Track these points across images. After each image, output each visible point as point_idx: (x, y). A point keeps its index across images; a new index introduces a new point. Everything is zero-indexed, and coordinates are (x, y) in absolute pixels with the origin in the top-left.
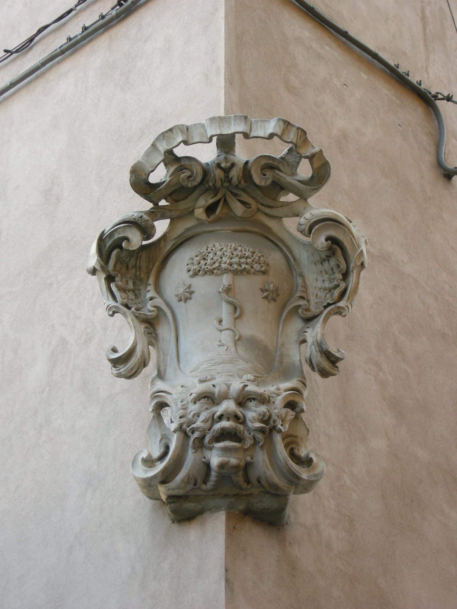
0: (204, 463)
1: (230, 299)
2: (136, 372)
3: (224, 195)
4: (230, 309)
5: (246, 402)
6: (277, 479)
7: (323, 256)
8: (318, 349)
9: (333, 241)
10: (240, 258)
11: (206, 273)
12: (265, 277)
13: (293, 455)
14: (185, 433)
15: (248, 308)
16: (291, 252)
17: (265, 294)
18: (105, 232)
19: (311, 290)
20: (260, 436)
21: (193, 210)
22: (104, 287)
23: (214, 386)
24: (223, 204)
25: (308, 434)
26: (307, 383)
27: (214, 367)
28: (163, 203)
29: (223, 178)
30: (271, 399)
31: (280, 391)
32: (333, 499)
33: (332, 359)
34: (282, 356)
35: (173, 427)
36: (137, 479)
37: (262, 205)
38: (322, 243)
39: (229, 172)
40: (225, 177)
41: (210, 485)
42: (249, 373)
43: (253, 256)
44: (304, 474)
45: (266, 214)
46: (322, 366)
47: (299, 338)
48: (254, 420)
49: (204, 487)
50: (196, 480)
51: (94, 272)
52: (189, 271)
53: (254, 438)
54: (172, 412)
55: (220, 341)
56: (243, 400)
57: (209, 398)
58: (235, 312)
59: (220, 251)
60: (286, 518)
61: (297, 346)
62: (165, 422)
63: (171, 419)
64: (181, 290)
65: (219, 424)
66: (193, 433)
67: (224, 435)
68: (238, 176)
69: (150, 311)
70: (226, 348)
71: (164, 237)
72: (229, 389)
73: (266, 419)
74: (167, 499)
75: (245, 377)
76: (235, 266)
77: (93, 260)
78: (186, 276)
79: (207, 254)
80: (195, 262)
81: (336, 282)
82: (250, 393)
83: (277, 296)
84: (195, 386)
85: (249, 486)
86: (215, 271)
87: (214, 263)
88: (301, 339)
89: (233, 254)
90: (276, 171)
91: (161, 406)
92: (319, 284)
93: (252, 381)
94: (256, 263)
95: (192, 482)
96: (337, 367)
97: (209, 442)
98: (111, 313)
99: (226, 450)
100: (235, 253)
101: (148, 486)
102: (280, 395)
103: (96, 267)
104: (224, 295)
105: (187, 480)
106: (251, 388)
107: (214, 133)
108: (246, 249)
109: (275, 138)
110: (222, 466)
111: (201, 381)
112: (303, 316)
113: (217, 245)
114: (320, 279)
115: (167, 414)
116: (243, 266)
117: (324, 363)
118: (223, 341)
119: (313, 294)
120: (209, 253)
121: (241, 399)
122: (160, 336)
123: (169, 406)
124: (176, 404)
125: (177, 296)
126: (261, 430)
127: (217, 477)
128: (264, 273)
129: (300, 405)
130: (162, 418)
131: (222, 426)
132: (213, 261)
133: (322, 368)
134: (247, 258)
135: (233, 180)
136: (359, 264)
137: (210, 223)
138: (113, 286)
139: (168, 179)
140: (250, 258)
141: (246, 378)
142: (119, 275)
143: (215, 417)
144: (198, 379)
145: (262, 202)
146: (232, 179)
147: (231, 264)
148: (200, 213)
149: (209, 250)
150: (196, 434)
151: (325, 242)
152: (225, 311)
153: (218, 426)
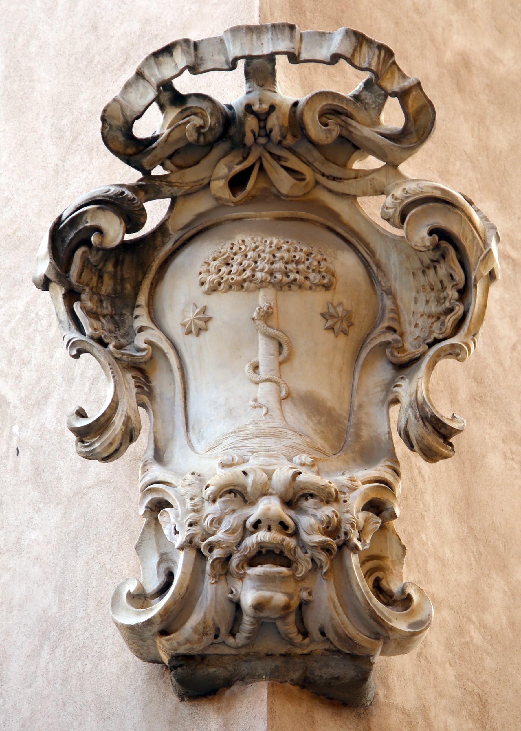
0: (231, 601)
1: (271, 331)
2: (116, 451)
3: (260, 158)
4: (273, 347)
5: (298, 500)
6: (353, 630)
7: (427, 261)
8: (418, 414)
9: (442, 235)
10: (287, 263)
11: (231, 287)
12: (328, 296)
13: (378, 589)
15: (301, 345)
16: (373, 254)
17: (330, 323)
18: (63, 218)
19: (405, 317)
20: (322, 557)
21: (209, 184)
22: (62, 308)
23: (245, 473)
24: (258, 174)
25: (404, 555)
26: (402, 472)
27: (245, 441)
28: (158, 171)
29: (257, 131)
30: (340, 495)
31: (355, 483)
32: (450, 665)
34: (358, 425)
35: (179, 540)
36: (122, 627)
37: (323, 175)
38: (423, 239)
39: (265, 120)
40: (260, 128)
41: (241, 638)
42: (304, 452)
43: (307, 260)
44: (400, 623)
45: (331, 191)
47: (387, 395)
48: (311, 531)
49: (231, 641)
50: (218, 630)
51: (45, 284)
52: (203, 284)
53: (312, 560)
54: (177, 516)
55: (256, 400)
57: (236, 493)
58: (280, 353)
59: (254, 250)
61: (385, 409)
62: (166, 531)
64: (190, 316)
65: (255, 535)
66: (211, 550)
67: (261, 555)
68: (281, 127)
69: (139, 350)
70: (264, 410)
71: (162, 229)
72: (270, 479)
74: (170, 662)
75: (297, 459)
76: (279, 276)
77: (43, 266)
78: (198, 292)
79: (232, 256)
80: (212, 269)
81: (447, 304)
82: (305, 485)
83: (349, 326)
84: (215, 474)
85: (307, 640)
86: (245, 285)
87: (244, 270)
88: (391, 397)
89: (274, 256)
90: (344, 118)
91: (159, 506)
92: (421, 307)
93: (308, 466)
94: (313, 271)
95: (212, 633)
96: (451, 445)
97: (237, 566)
98: (74, 352)
99: (265, 580)
100: (278, 255)
101: (135, 634)
102: (355, 489)
103: (49, 276)
104: (260, 323)
105: (202, 631)
106: (307, 477)
107: (238, 54)
108: (296, 248)
109: (342, 61)
111: (223, 465)
112: (394, 360)
113: (248, 240)
114: (422, 298)
115: (168, 519)
116: (292, 276)
117: (429, 438)
118: (260, 401)
119: (410, 324)
120: (235, 254)
121: (290, 495)
122: (157, 391)
123: (172, 507)
124: (183, 504)
125: (184, 325)
126: (326, 548)
127: (252, 624)
128: (327, 287)
129: (389, 506)
131: (259, 539)
132: (241, 268)
134: (297, 263)
135: (273, 134)
136: (486, 273)
137: (236, 204)
138: (77, 307)
139: (166, 131)
140: (304, 262)
141: (298, 461)
142: (87, 289)
143: (248, 524)
144: (219, 461)
145: (323, 170)
146: (271, 131)
147: (271, 273)
148: (219, 187)
149: (235, 248)
150: (217, 553)
151: (428, 237)
152: (263, 352)
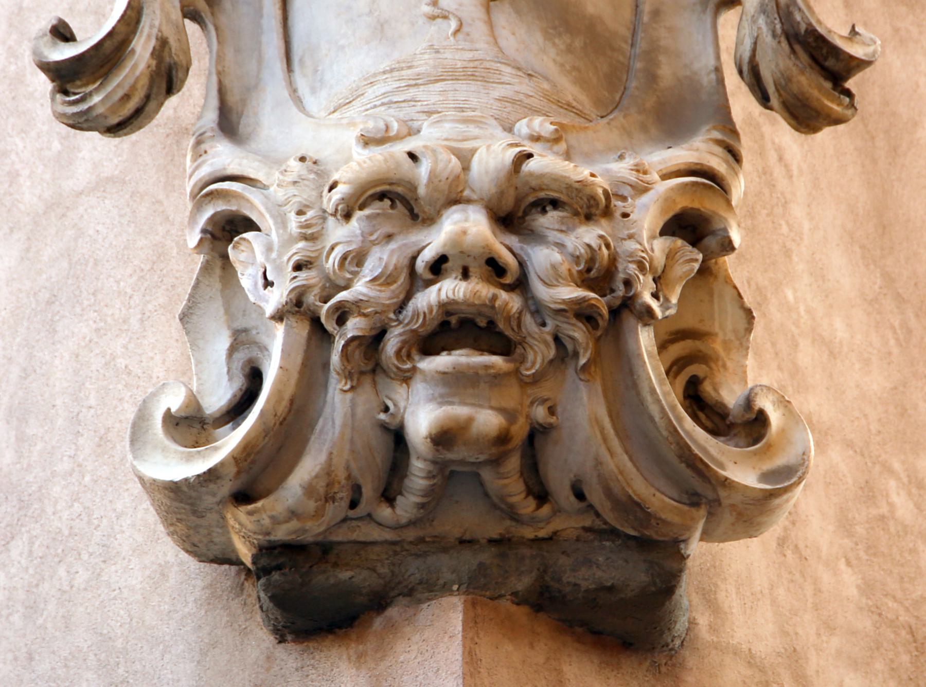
0: (384, 427)
5: (526, 213)
8: (778, 26)
13: (697, 400)
14: (315, 322)
20: (578, 333)
23: (413, 156)
25: (749, 330)
30: (615, 202)
32: (848, 563)
33: (830, 63)
34: (652, 55)
35: (275, 299)
36: (154, 487)
41: (407, 505)
44: (742, 472)
46: (795, 88)
48: (554, 278)
49: (385, 512)
50: (357, 489)
53: (557, 339)
54: (269, 249)
56: (519, 208)
57: (394, 200)
60: (681, 626)
62: (246, 282)
63: (264, 269)
65: (434, 288)
66: (341, 321)
67: (451, 329)
70: (453, 24)
72: (466, 168)
73: (598, 273)
75: (523, 127)
82: (542, 181)
84: (348, 160)
85: (546, 510)
91: (229, 228)
93: (547, 140)
95: (344, 495)
96: (848, 93)
97: (398, 353)
99: (456, 383)
101: (182, 504)
102: (645, 190)
105: (323, 492)
106: (544, 163)
110: (443, 438)
111: (367, 141)
115: (250, 256)
117: (803, 80)
121: (508, 203)
123: (259, 230)
124: (282, 222)
126: (584, 314)
127: (430, 476)
130: (235, 272)
131: (443, 296)
133: (795, 97)
143: (420, 264)
144: (356, 132)
150: (354, 326)
153: (429, 298)
